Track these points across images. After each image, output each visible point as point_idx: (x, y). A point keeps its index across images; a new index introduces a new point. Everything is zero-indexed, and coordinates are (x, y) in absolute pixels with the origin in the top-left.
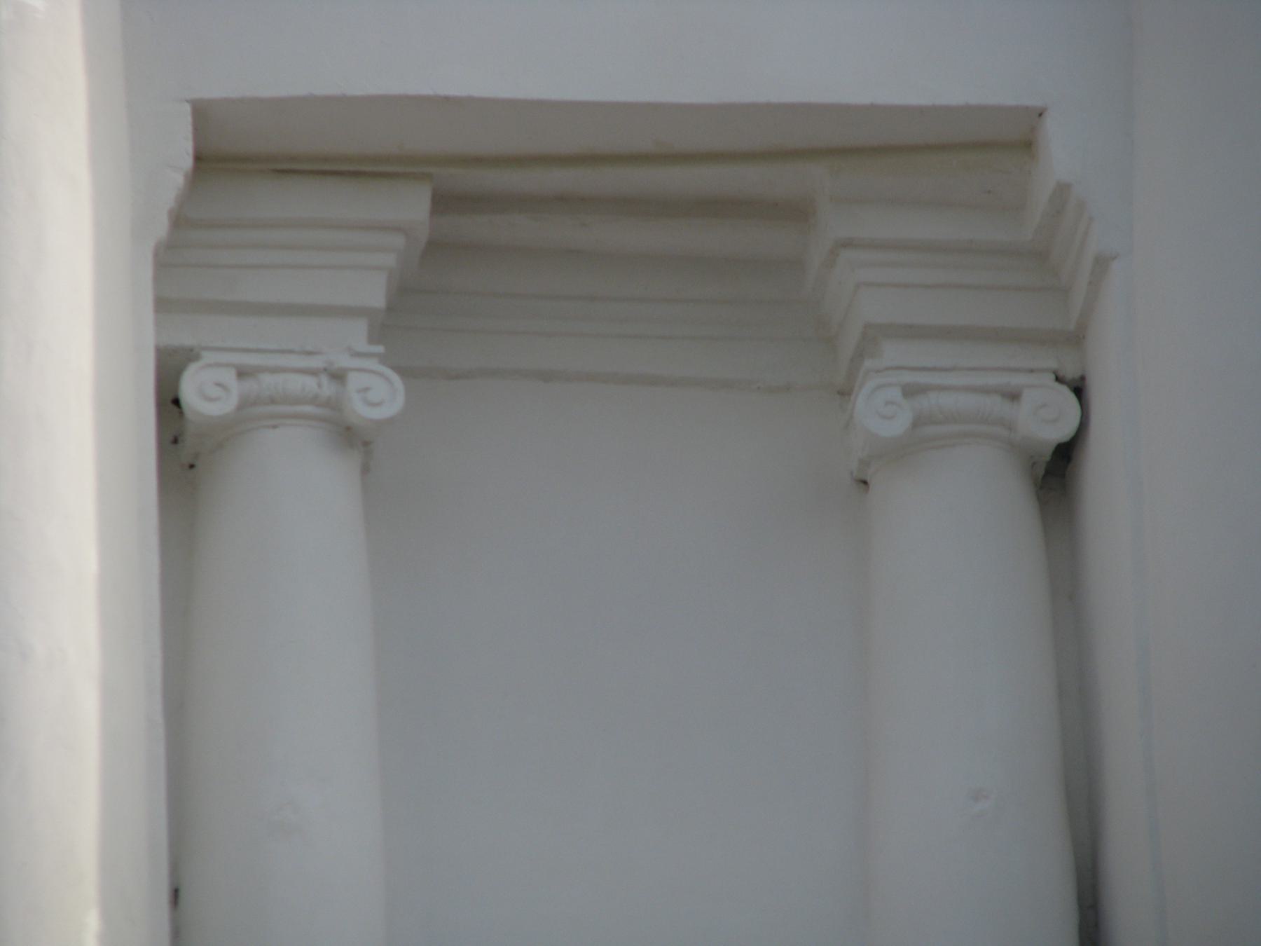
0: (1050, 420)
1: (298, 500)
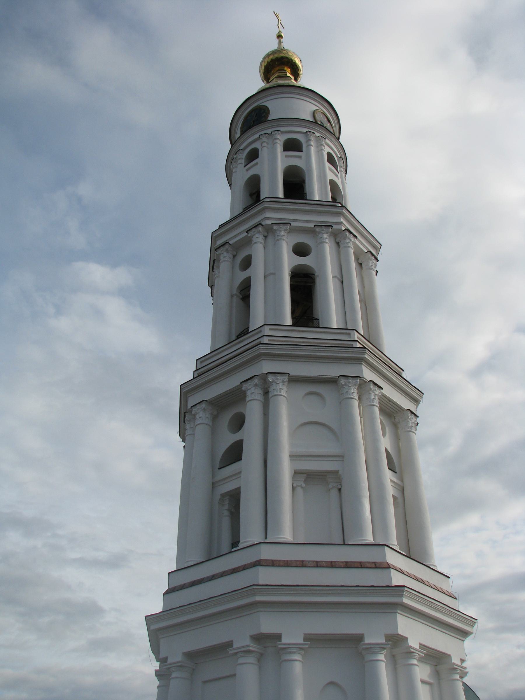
0: (339, 487)
1: (299, 491)
